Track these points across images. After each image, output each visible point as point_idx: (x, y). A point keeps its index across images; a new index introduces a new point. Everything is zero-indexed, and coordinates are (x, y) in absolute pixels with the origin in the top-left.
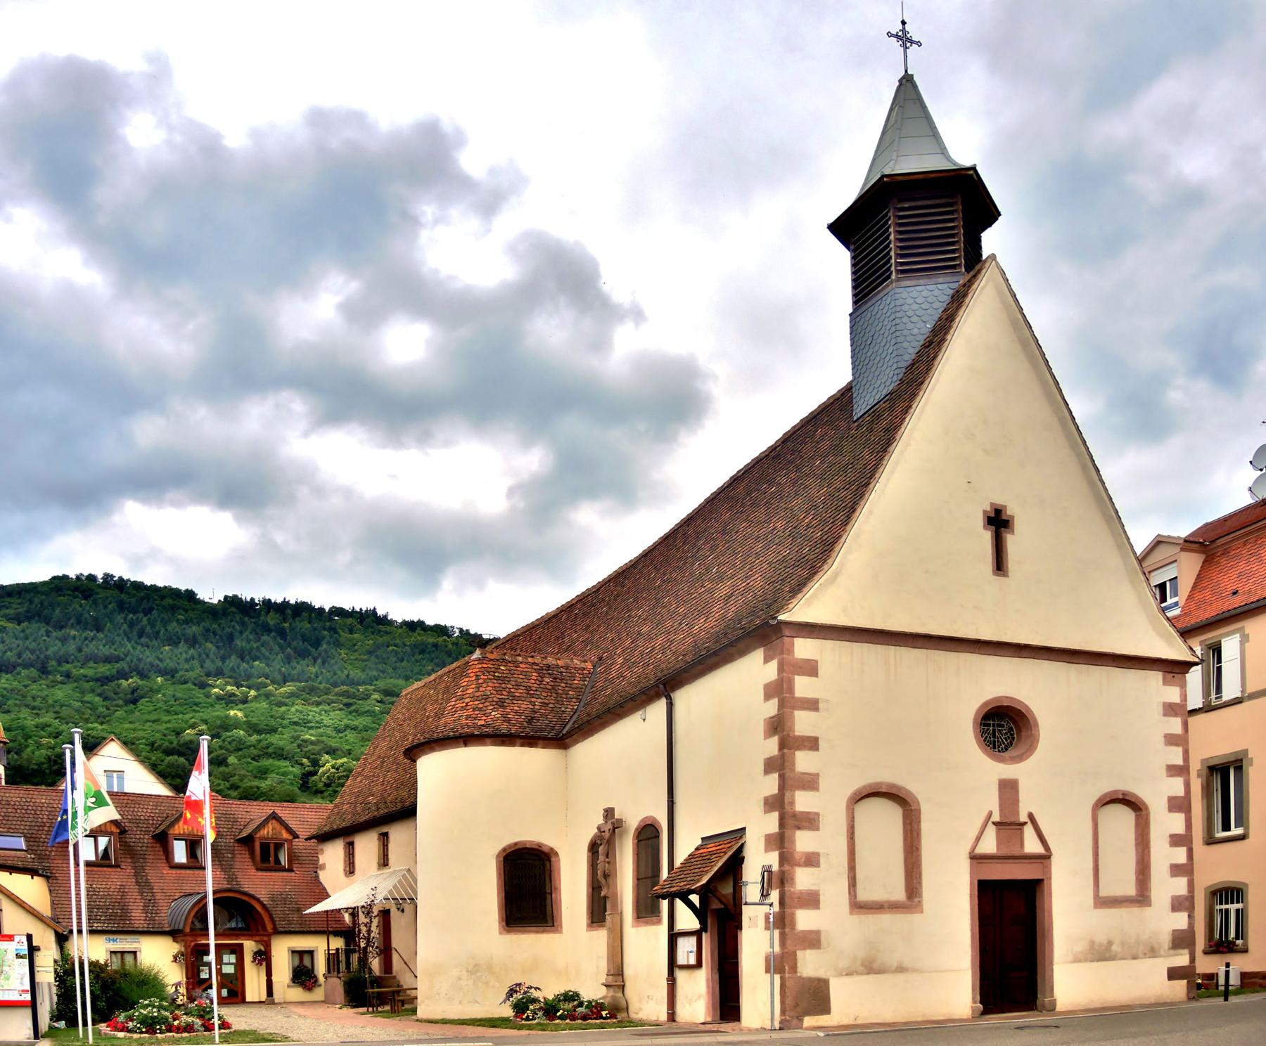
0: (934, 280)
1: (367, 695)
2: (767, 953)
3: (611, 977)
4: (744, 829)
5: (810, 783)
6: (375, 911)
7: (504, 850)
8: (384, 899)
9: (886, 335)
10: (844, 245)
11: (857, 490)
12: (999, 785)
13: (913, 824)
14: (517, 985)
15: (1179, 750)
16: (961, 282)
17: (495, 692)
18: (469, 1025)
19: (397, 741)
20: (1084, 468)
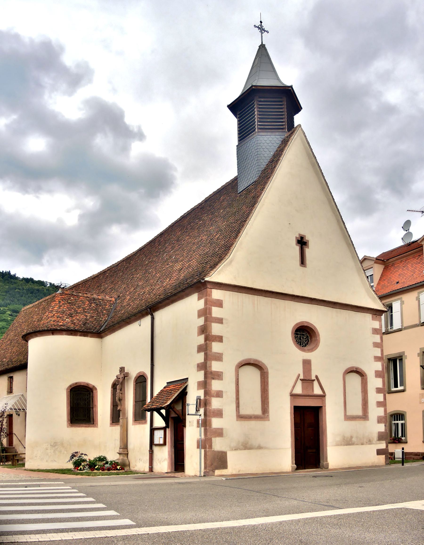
0: (274, 134)
1: (4, 312)
2: (198, 439)
3: (121, 449)
4: (187, 378)
5: (219, 357)
6: (6, 415)
7: (70, 386)
8: (10, 409)
9: (253, 156)
10: (235, 116)
11: (240, 223)
12: (303, 362)
13: (265, 379)
14: (75, 453)
15: (379, 350)
16: (286, 135)
17: (68, 310)
18: (51, 472)
19: (18, 333)
20: (338, 221)
